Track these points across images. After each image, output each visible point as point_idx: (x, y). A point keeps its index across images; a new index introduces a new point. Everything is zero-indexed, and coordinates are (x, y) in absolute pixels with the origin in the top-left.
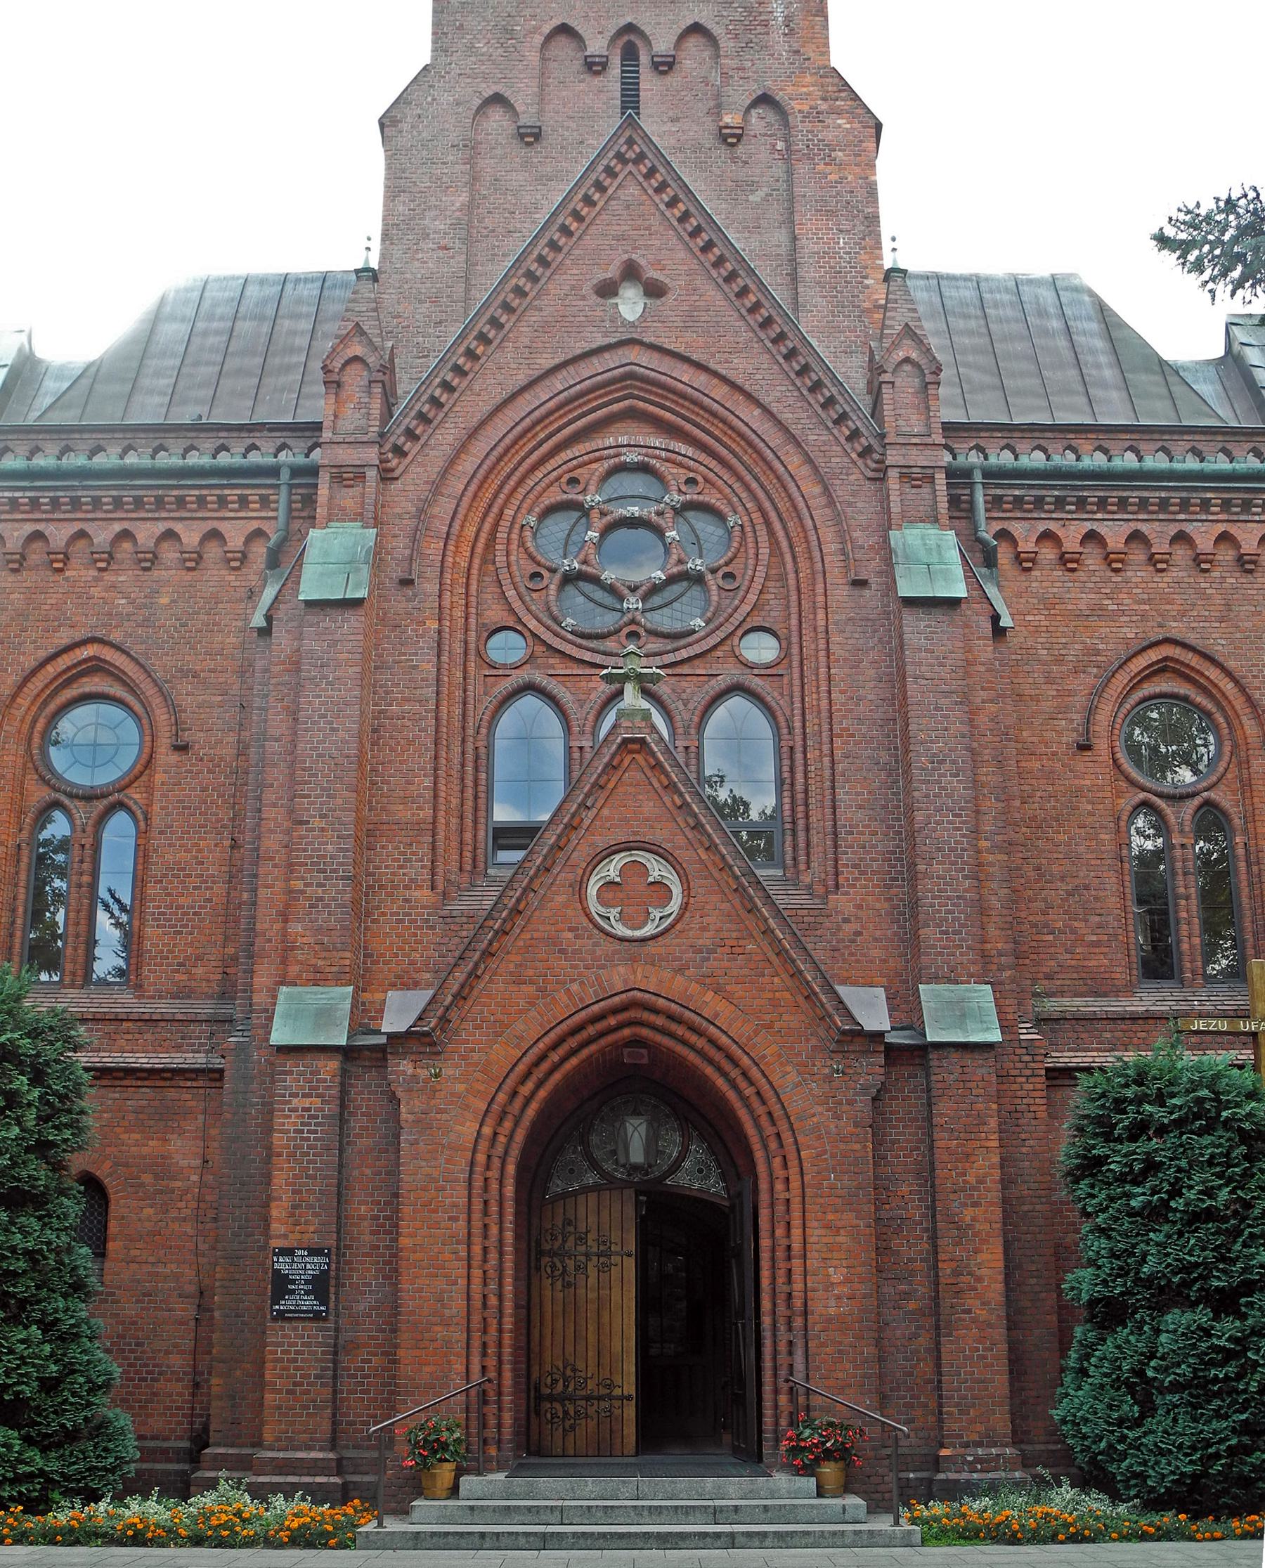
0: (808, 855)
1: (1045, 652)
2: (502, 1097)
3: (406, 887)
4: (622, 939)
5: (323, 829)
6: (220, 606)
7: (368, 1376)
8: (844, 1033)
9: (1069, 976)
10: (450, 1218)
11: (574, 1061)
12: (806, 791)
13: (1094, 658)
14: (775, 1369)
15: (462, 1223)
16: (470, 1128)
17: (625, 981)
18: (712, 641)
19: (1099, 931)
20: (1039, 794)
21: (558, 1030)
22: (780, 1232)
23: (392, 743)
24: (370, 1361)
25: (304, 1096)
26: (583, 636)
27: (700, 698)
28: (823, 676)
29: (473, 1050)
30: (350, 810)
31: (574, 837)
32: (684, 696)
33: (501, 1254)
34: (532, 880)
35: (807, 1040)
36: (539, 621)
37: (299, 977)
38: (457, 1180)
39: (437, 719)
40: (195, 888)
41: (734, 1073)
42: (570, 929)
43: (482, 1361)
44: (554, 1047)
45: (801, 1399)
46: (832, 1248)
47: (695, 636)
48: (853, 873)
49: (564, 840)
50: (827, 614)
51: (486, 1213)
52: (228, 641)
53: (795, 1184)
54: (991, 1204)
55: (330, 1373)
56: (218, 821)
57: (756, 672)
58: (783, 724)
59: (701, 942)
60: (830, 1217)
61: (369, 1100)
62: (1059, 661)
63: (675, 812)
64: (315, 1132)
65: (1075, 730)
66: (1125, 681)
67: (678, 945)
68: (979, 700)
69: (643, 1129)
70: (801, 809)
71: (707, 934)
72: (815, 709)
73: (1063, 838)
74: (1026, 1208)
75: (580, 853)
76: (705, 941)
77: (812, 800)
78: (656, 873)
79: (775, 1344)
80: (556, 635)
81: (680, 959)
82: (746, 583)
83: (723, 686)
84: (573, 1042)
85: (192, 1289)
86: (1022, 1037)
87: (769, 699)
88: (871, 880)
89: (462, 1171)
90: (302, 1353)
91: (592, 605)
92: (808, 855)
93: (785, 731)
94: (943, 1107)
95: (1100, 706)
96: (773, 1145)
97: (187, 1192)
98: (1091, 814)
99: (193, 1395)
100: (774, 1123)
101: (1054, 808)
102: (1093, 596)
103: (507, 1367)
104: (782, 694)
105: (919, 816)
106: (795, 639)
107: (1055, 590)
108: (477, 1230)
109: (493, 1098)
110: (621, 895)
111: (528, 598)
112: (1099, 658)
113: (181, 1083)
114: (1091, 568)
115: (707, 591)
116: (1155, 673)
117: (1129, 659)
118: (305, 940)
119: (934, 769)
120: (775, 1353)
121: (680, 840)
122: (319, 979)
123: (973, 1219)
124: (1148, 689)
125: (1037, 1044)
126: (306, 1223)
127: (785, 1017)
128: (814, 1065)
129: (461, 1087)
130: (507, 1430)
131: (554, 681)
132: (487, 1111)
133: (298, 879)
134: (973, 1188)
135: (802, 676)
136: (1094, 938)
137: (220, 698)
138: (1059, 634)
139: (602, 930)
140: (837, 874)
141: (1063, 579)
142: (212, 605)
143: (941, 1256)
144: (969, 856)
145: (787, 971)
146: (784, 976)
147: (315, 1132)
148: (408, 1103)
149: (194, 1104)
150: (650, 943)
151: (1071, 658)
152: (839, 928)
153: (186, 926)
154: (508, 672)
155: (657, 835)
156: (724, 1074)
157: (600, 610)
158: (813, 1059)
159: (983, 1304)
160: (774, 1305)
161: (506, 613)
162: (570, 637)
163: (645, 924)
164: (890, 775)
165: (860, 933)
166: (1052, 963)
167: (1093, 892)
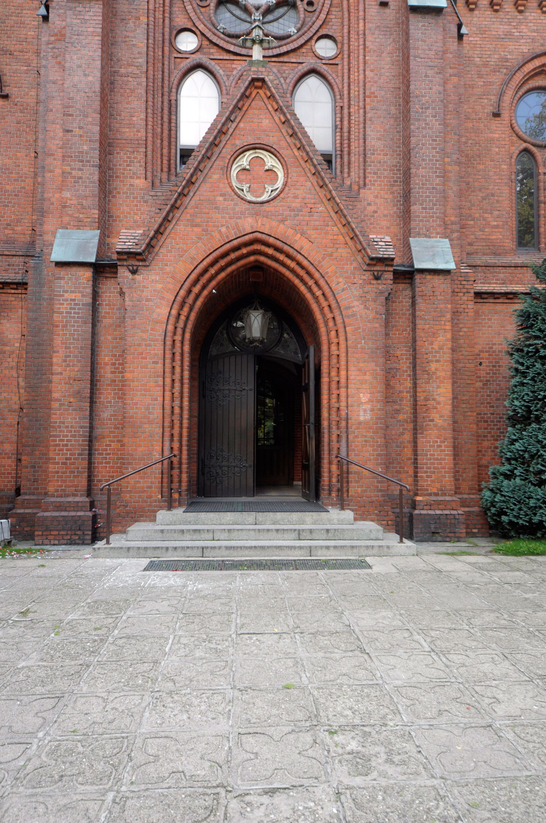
0: (349, 168)
1: (478, 59)
2: (182, 293)
3: (131, 177)
4: (250, 202)
5: (81, 136)
6: (24, 12)
7: (109, 454)
8: (372, 259)
9: (481, 244)
10: (154, 363)
11: (223, 275)
12: (349, 132)
13: (505, 64)
14: (330, 450)
15: (160, 365)
16: (165, 311)
17: (252, 227)
18: (301, 41)
19: (498, 219)
20: (470, 142)
21: (215, 255)
22: (334, 373)
23: (122, 91)
24: (110, 445)
25: (72, 292)
26: (230, 36)
27: (293, 76)
28: (361, 61)
29: (166, 265)
30: (96, 125)
31: (224, 139)
32: (284, 75)
33: (182, 384)
34: (200, 163)
35: (351, 264)
36: (205, 25)
37: (69, 224)
38: (157, 340)
39: (147, 78)
40: (15, 180)
41: (311, 283)
42: (222, 195)
43: (171, 444)
44: (212, 264)
45: (345, 467)
46: (363, 382)
47: (291, 39)
48: (373, 177)
49: (218, 139)
50: (365, 23)
51: (173, 360)
52: (29, 33)
53: (343, 346)
54: (446, 361)
55: (87, 452)
56: (27, 141)
57: (324, 62)
58: (337, 93)
59: (293, 205)
60: (361, 365)
61: (110, 296)
62: (486, 65)
63: (281, 126)
64: (78, 313)
65: (491, 105)
66: (521, 78)
67: (282, 206)
68: (448, 75)
69: (259, 318)
70: (346, 142)
71: (297, 200)
72: (356, 82)
73: (481, 167)
74: (462, 365)
75: (228, 152)
76: (296, 204)
77: (352, 136)
78: (269, 164)
79: (330, 436)
80: (215, 34)
81: (282, 214)
82: (320, 7)
83: (306, 69)
84: (223, 263)
85: (17, 407)
86: (462, 271)
87: (330, 78)
88: (383, 181)
89: (160, 335)
90: (70, 441)
91: (234, 18)
92: (349, 168)
93: (338, 97)
94: (421, 305)
95: (507, 91)
96: (331, 324)
97: (12, 352)
98: (497, 154)
99: (17, 466)
100: (331, 311)
101: (478, 150)
102: (506, 27)
103: (185, 448)
104: (337, 76)
105: (413, 140)
106: (346, 41)
107: (486, 23)
108: (168, 370)
109: (178, 293)
110: (249, 177)
111: (198, 11)
112: (508, 64)
113: (9, 291)
114: (507, 10)
115: (298, 12)
116: (536, 74)
117: (524, 65)
118: (72, 202)
119: (422, 112)
120: (330, 441)
121: (283, 144)
122: (80, 225)
123: (436, 369)
124: (532, 84)
125: (470, 275)
126: (73, 365)
127: (339, 250)
128: (355, 278)
129: (159, 286)
130: (184, 484)
131: (213, 63)
132: (174, 301)
133: (67, 165)
134: (436, 352)
135: (349, 63)
136: (495, 223)
137: (26, 68)
138: (487, 49)
139: (239, 196)
140: (365, 178)
141: (491, 16)
142: (19, 11)
143: (419, 389)
144: (440, 165)
145: (341, 223)
146: (340, 226)
147: (78, 313)
148: (129, 295)
149: (16, 303)
150: (265, 205)
151: (492, 63)
152: (365, 209)
153: (10, 202)
154: (187, 56)
155: (271, 140)
156: (305, 284)
157: (238, 21)
158: (354, 274)
159: (441, 416)
160: (329, 415)
161: (186, 21)
162: (222, 36)
163: (262, 194)
164: (396, 121)
165: (376, 212)
166: (473, 237)
167: (496, 198)
